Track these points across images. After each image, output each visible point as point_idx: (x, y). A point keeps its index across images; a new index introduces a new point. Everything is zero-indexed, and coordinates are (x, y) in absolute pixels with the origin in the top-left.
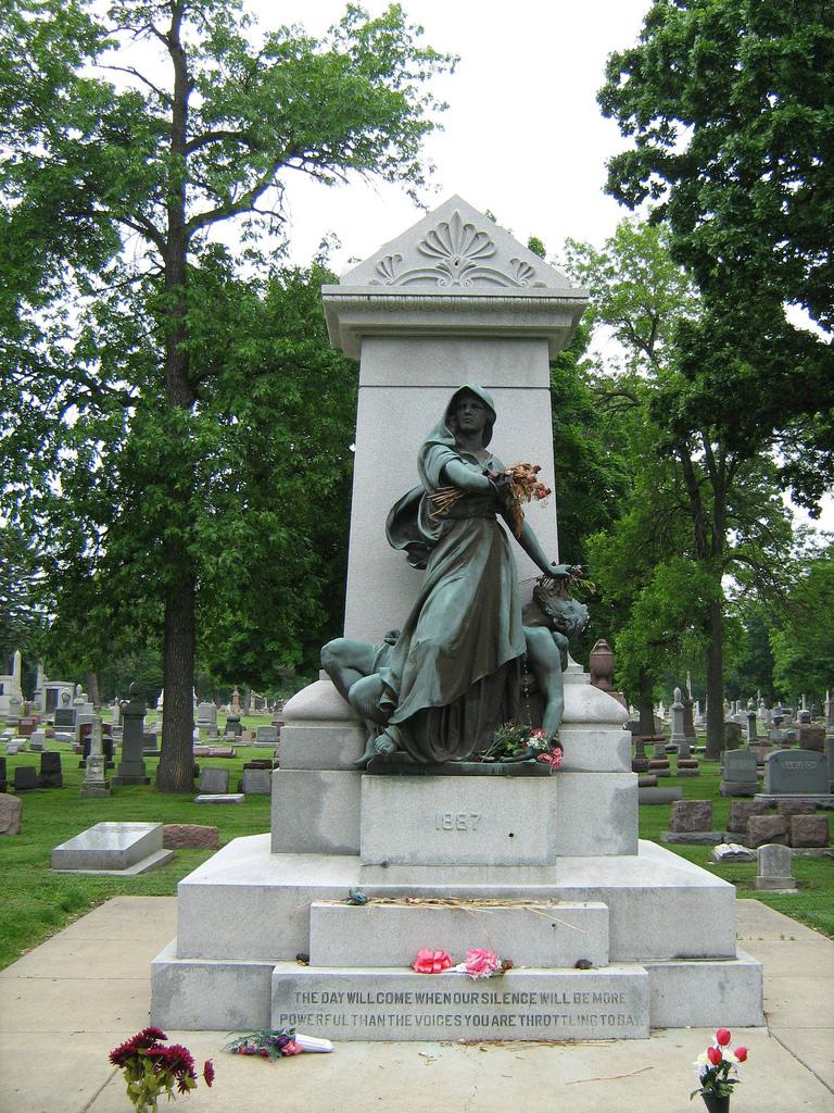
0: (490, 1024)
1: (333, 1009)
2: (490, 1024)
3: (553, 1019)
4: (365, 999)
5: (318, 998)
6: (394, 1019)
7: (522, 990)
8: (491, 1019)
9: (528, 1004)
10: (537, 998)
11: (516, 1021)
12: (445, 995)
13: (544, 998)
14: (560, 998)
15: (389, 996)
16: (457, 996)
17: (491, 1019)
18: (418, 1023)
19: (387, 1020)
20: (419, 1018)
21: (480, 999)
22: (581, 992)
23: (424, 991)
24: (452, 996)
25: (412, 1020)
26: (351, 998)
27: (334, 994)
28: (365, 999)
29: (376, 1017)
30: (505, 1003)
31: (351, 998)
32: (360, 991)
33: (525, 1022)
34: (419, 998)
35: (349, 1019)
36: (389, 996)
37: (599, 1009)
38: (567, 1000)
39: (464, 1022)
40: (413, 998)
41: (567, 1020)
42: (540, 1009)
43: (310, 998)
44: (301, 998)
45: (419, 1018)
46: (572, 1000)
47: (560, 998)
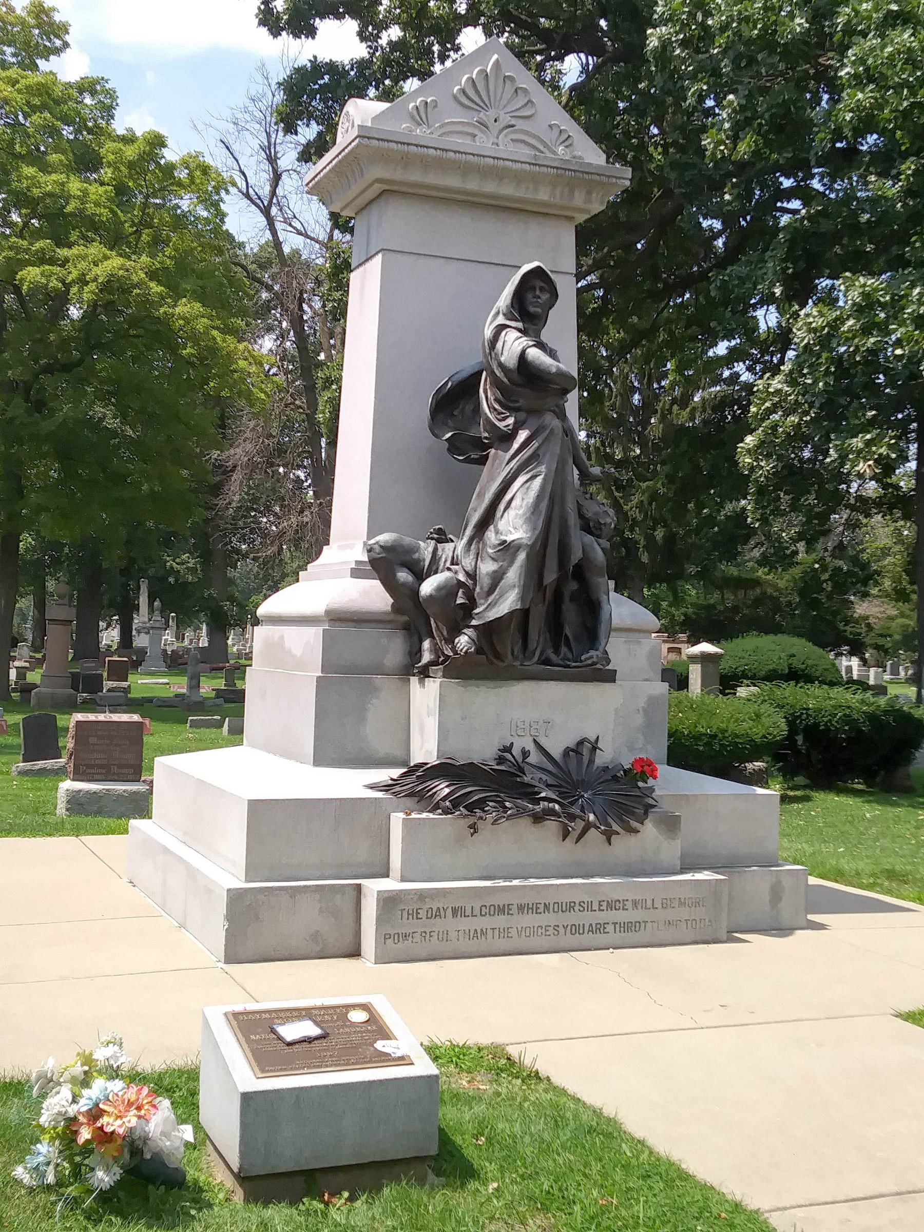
1: (438, 925)
3: (643, 925)
4: (468, 912)
5: (422, 914)
6: (496, 932)
8: (586, 928)
9: (621, 911)
10: (629, 905)
13: (635, 904)
15: (492, 908)
16: (556, 905)
17: (586, 928)
18: (519, 935)
19: (490, 932)
20: (520, 929)
22: (668, 897)
25: (514, 932)
26: (455, 912)
28: (468, 912)
29: (479, 931)
30: (600, 910)
31: (455, 912)
34: (521, 908)
35: (453, 935)
36: (492, 908)
37: (684, 913)
39: (562, 930)
40: (514, 910)
41: (655, 925)
43: (415, 914)
44: (405, 915)
45: (520, 929)
47: (649, 903)
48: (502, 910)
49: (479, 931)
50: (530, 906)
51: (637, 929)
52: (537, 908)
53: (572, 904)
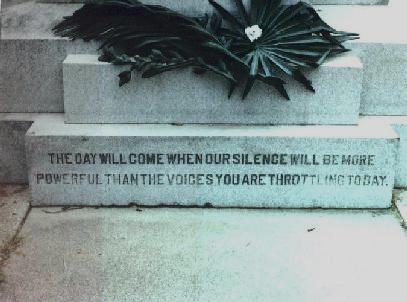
0: (241, 182)
1: (88, 169)
2: (241, 182)
6: (147, 178)
7: (273, 151)
10: (287, 159)
11: (266, 180)
12: (265, 156)
13: (294, 160)
14: (310, 159)
21: (231, 160)
23: (175, 152)
24: (204, 158)
27: (87, 156)
29: (129, 177)
30: (256, 163)
32: (111, 152)
33: (275, 181)
34: (172, 158)
35: (103, 178)
38: (317, 160)
39: (216, 180)
40: (164, 159)
42: (290, 169)
45: (171, 177)
46: (321, 162)
47: (310, 159)
48: (151, 159)
49: (129, 177)
50: (181, 157)
51: (295, 182)
52: (159, 159)
53: (226, 157)
